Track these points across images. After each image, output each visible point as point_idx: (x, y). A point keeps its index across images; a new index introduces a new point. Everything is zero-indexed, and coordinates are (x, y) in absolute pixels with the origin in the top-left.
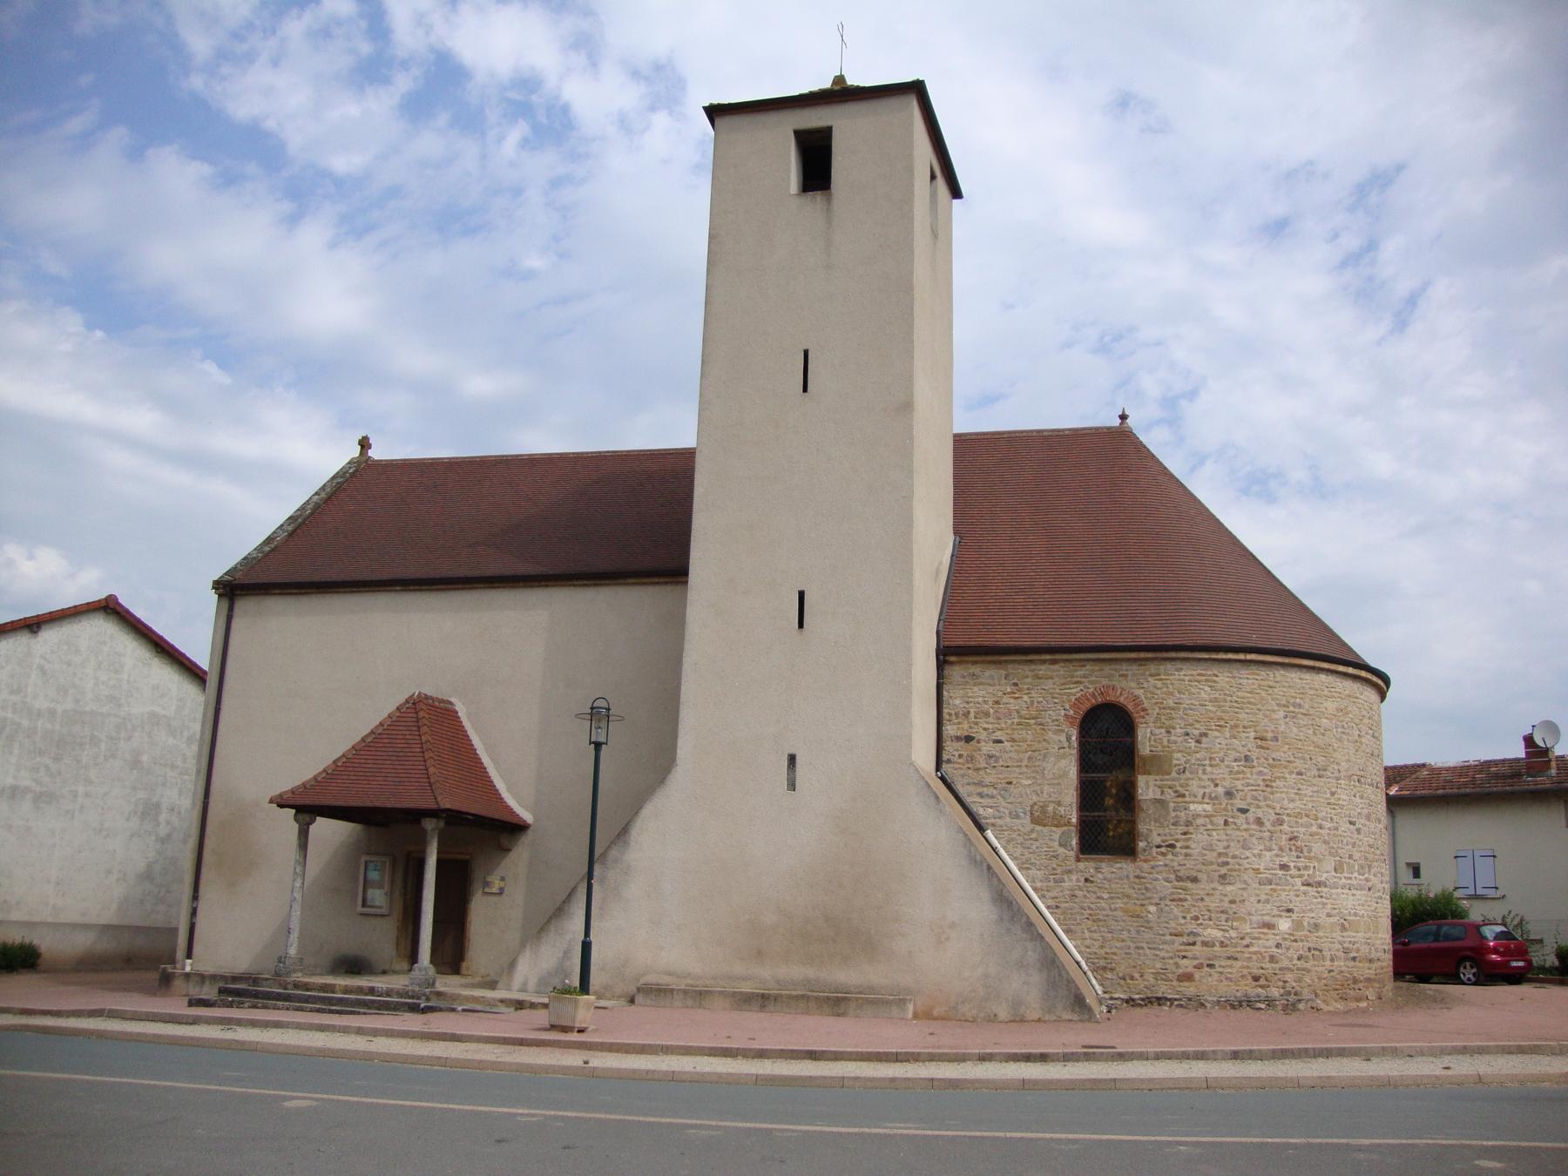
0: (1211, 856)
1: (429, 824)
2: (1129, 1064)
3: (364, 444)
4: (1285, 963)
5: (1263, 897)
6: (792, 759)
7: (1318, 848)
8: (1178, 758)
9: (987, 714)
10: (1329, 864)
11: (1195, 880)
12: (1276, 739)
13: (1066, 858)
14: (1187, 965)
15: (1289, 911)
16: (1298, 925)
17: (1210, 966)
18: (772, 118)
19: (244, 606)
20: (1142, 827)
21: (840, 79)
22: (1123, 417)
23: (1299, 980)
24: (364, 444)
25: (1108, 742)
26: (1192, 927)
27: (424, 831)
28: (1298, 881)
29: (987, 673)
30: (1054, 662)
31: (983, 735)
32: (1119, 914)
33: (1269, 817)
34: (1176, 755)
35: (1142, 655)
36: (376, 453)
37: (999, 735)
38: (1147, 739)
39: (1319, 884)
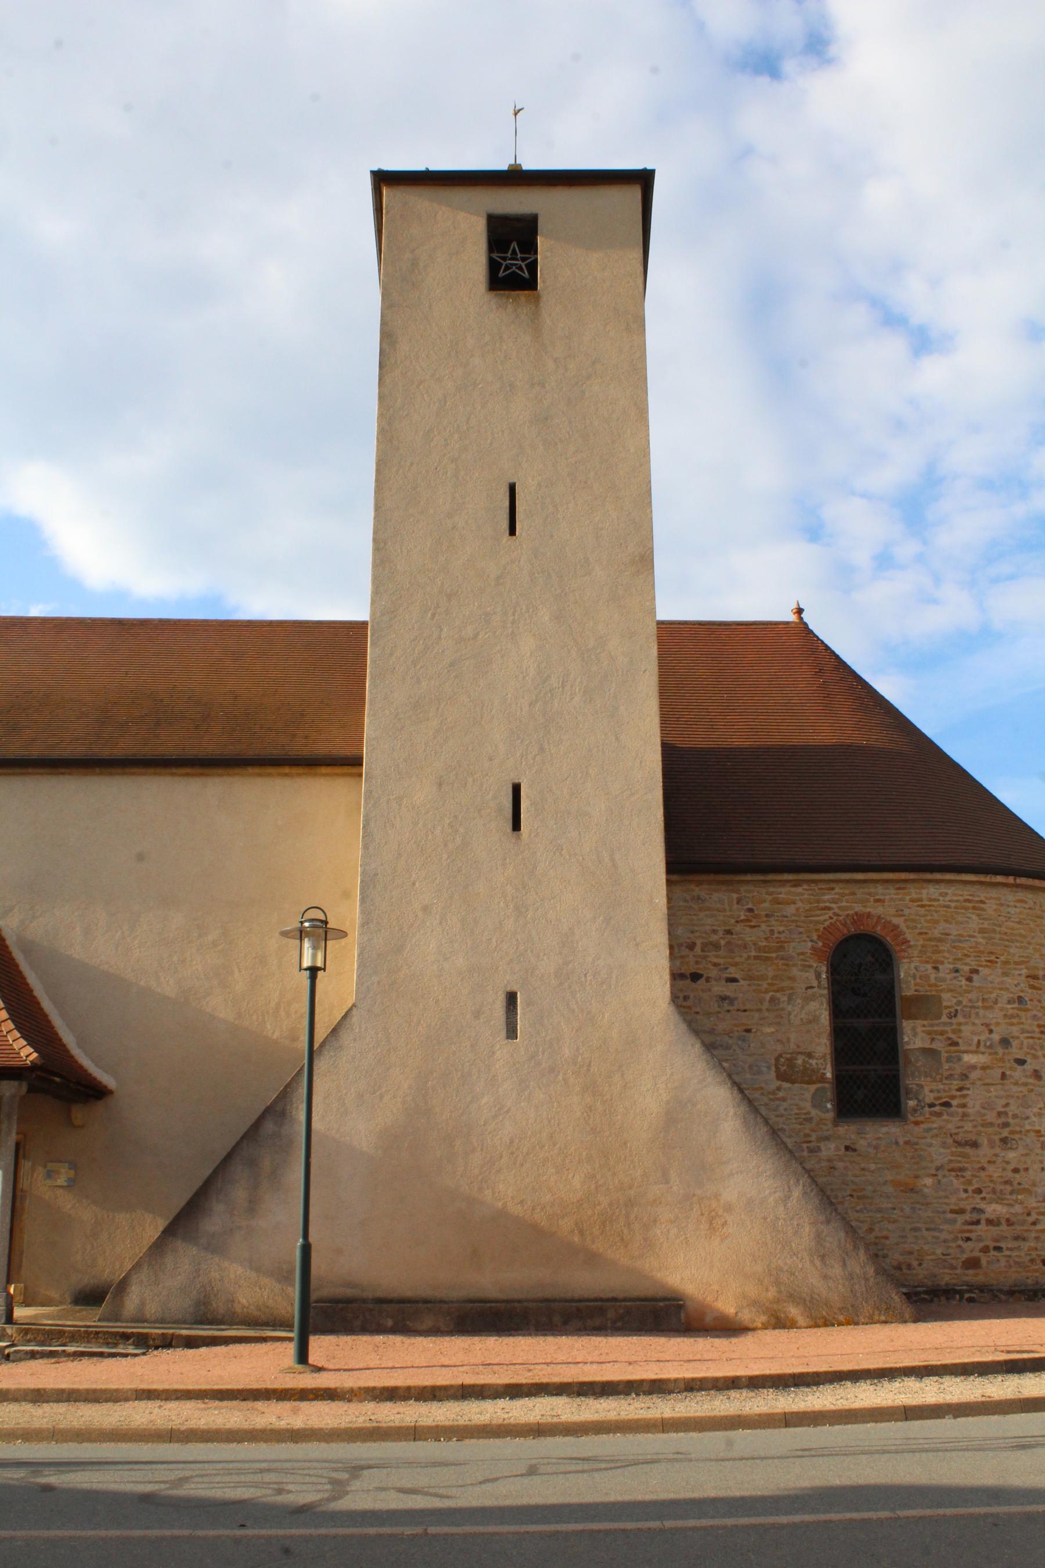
0: (991, 1117)
2: (897, 1384)
6: (511, 999)
8: (948, 999)
11: (975, 1145)
14: (971, 1249)
17: (998, 1249)
20: (909, 1082)
22: (799, 611)
25: (864, 982)
26: (977, 1201)
29: (716, 896)
30: (797, 884)
31: (714, 973)
32: (889, 1189)
34: (945, 996)
35: (903, 876)
37: (732, 972)
38: (911, 974)
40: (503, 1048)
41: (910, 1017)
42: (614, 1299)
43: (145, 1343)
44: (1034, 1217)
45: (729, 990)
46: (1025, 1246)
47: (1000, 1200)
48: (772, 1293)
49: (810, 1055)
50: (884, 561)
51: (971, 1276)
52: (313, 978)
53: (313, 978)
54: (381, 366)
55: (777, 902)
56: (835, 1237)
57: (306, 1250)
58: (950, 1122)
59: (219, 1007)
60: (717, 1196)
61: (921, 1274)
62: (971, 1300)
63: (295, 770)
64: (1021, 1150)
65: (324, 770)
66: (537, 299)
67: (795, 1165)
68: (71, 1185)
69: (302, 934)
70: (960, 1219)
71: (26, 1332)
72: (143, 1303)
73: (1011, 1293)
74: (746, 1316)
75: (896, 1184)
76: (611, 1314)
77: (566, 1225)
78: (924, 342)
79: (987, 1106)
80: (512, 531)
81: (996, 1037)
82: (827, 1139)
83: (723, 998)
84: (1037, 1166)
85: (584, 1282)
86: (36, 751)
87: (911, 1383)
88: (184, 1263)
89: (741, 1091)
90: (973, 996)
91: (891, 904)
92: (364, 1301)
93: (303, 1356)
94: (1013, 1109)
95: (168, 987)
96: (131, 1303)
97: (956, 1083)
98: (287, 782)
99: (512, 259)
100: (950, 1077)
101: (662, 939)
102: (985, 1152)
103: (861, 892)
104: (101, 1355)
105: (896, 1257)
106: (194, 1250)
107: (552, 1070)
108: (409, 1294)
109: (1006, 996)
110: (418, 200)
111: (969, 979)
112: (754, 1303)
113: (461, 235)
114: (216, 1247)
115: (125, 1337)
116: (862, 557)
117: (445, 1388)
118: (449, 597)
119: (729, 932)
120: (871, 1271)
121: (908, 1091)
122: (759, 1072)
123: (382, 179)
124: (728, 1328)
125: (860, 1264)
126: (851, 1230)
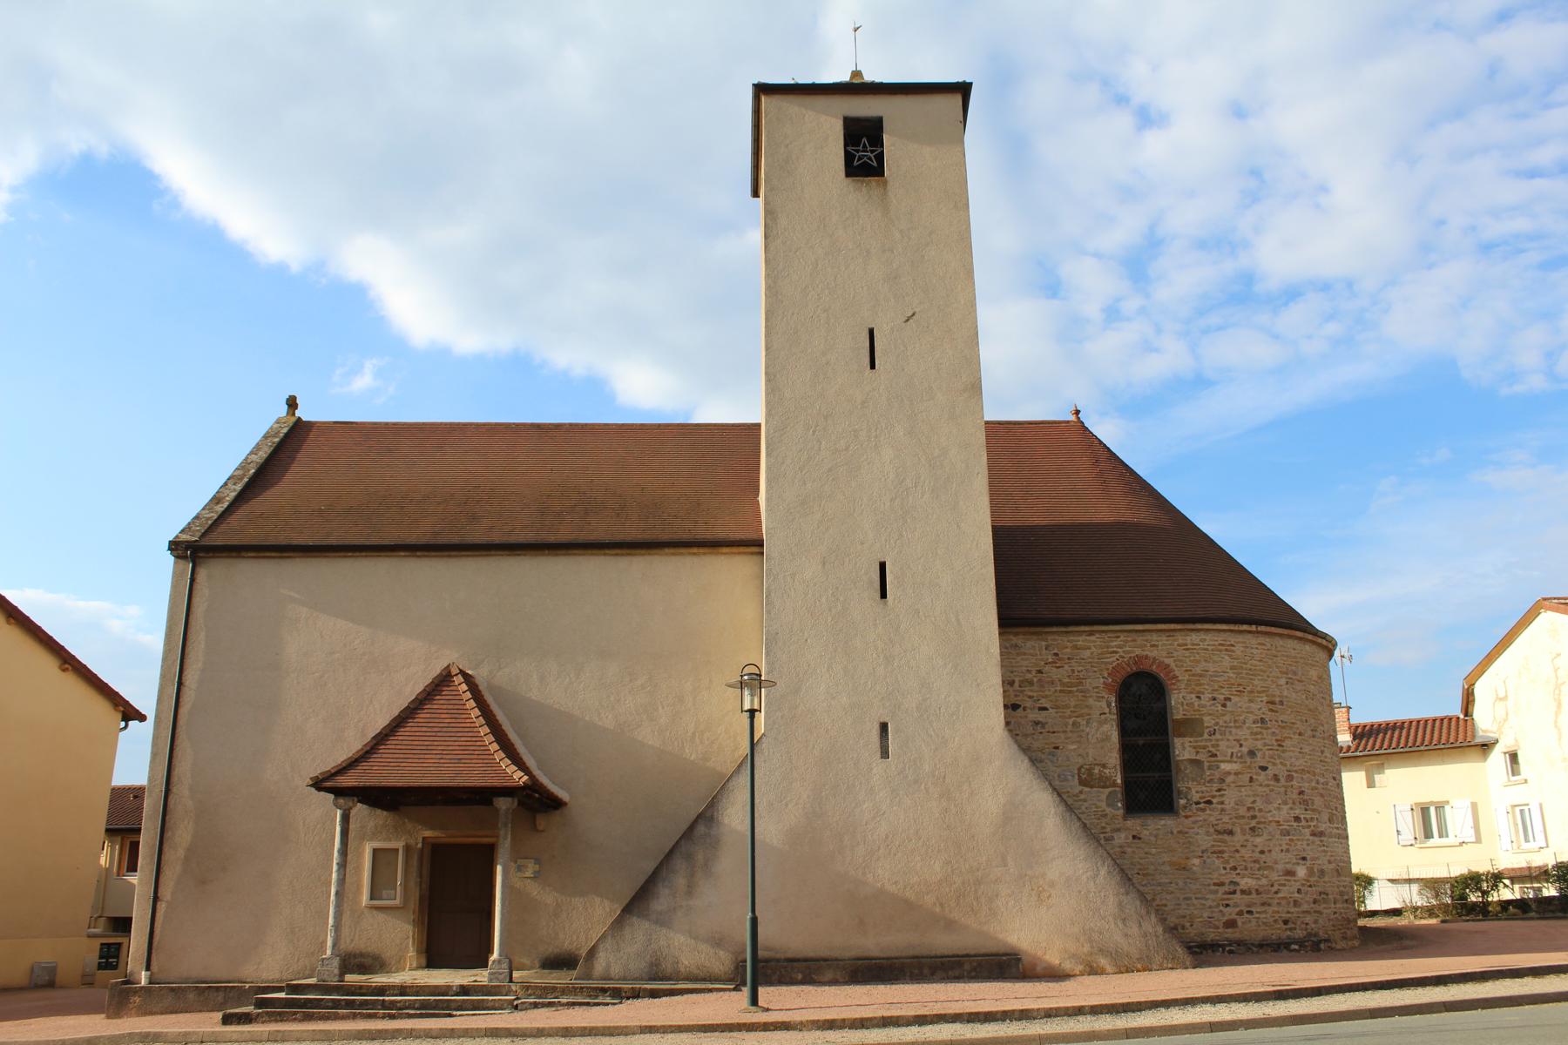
0: (1242, 811)
1: (503, 804)
2: (1198, 1009)
3: (292, 403)
4: (1305, 907)
5: (1285, 847)
6: (884, 727)
7: (1318, 802)
8: (1208, 721)
9: (1031, 683)
10: (1325, 817)
11: (1231, 833)
12: (1281, 703)
13: (1114, 817)
14: (1230, 913)
15: (1304, 859)
16: (1311, 871)
17: (1249, 912)
18: (821, 101)
19: (213, 573)
20: (1181, 785)
21: (856, 74)
22: (1077, 412)
23: (1316, 922)
24: (292, 403)
25: (1144, 707)
26: (1233, 876)
27: (497, 810)
28: (1307, 831)
29: (1029, 644)
30: (1091, 633)
31: (1029, 704)
32: (1167, 868)
33: (1282, 775)
34: (1206, 719)
35: (1172, 626)
36: (304, 413)
37: (1044, 703)
38: (1179, 702)
39: (1321, 834)
40: (879, 766)
41: (1180, 735)
42: (968, 955)
43: (619, 995)
44: (1276, 888)
45: (1041, 716)
46: (1270, 910)
47: (1252, 876)
48: (1086, 949)
49: (1104, 766)
50: (1113, 314)
51: (1230, 934)
52: (752, 717)
53: (752, 717)
54: (766, 237)
55: (1076, 647)
56: (1133, 905)
57: (754, 921)
58: (1211, 816)
59: (648, 736)
60: (1043, 875)
61: (1192, 932)
62: (1231, 952)
63: (701, 550)
64: (1265, 836)
65: (725, 550)
66: (885, 183)
67: (1101, 850)
68: (536, 876)
69: (742, 685)
70: (1222, 889)
71: (527, 988)
72: (608, 966)
73: (1261, 946)
74: (1068, 966)
75: (1171, 864)
76: (967, 967)
77: (929, 900)
78: (1147, 118)
79: (1239, 803)
80: (873, 366)
81: (1245, 750)
82: (1118, 830)
83: (1037, 723)
84: (1278, 849)
85: (944, 943)
86: (496, 538)
87: (1208, 1007)
88: (639, 932)
89: (1059, 795)
90: (1227, 718)
91: (1165, 648)
92: (778, 960)
93: (754, 1001)
94: (1259, 805)
95: (608, 721)
96: (600, 966)
97: (1216, 786)
98: (695, 559)
99: (864, 151)
100: (1211, 781)
101: (996, 680)
102: (1239, 838)
103: (1140, 639)
104: (588, 1004)
105: (1172, 920)
106: (646, 925)
107: (916, 782)
108: (811, 954)
109: (1252, 717)
110: (790, 105)
111: (1224, 705)
112: (1074, 956)
113: (823, 134)
114: (664, 921)
115: (604, 990)
116: (1093, 310)
117: (871, 1019)
118: (826, 418)
119: (1040, 672)
120: (1160, 930)
121: (1179, 792)
122: (1066, 780)
123: (761, 90)
124: (1055, 975)
125: (1152, 925)
126: (1142, 896)
